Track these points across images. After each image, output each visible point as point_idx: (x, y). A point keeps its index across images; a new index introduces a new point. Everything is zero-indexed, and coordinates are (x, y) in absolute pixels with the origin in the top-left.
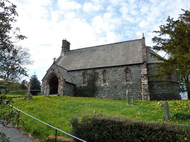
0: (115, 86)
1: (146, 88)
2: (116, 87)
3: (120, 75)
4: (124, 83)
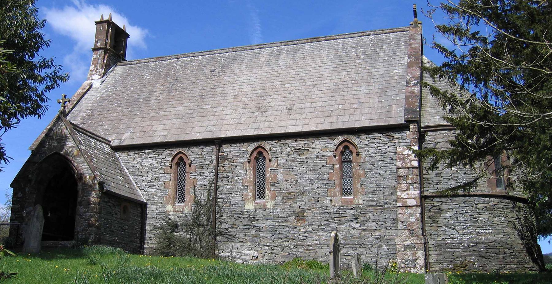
0: (298, 211)
1: (412, 219)
2: (300, 216)
3: (317, 168)
4: (334, 199)
